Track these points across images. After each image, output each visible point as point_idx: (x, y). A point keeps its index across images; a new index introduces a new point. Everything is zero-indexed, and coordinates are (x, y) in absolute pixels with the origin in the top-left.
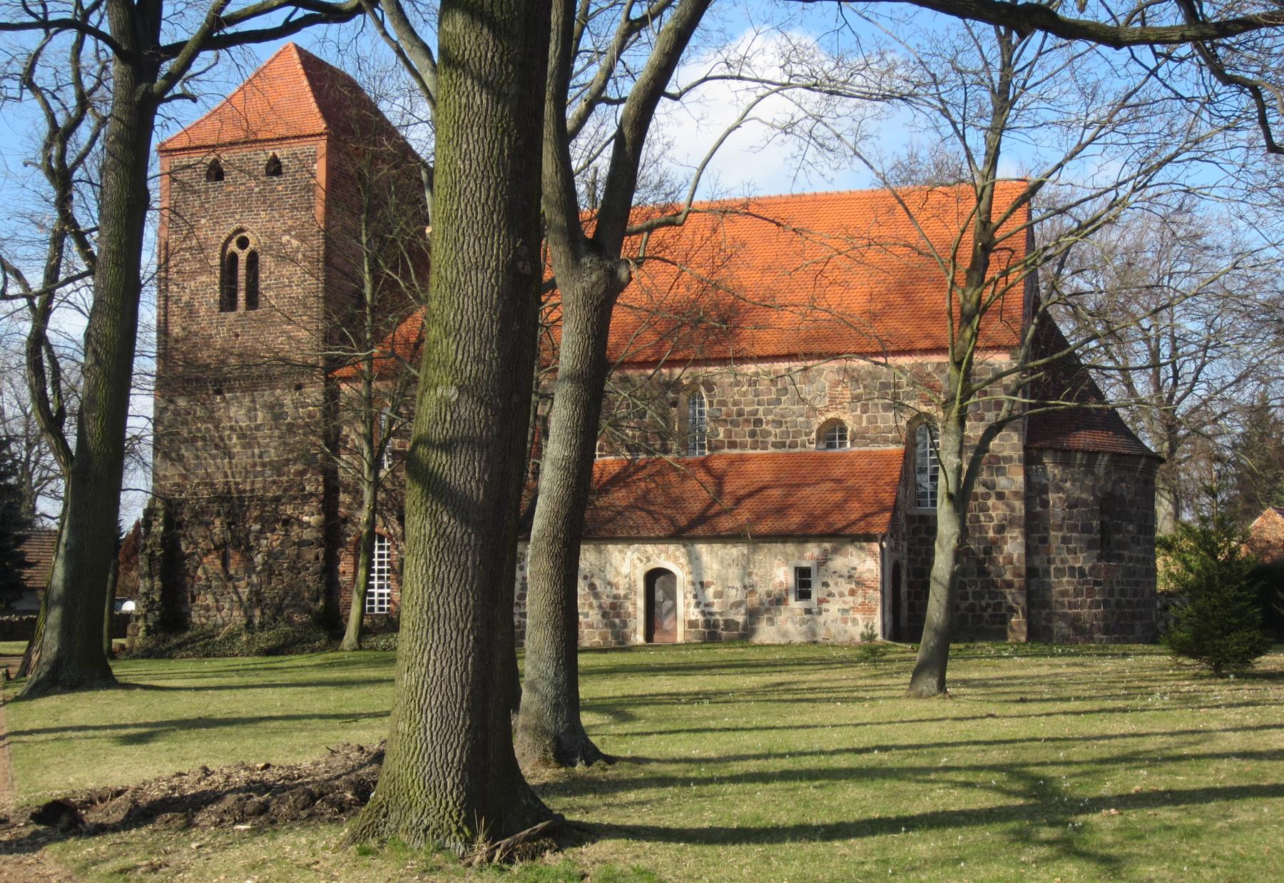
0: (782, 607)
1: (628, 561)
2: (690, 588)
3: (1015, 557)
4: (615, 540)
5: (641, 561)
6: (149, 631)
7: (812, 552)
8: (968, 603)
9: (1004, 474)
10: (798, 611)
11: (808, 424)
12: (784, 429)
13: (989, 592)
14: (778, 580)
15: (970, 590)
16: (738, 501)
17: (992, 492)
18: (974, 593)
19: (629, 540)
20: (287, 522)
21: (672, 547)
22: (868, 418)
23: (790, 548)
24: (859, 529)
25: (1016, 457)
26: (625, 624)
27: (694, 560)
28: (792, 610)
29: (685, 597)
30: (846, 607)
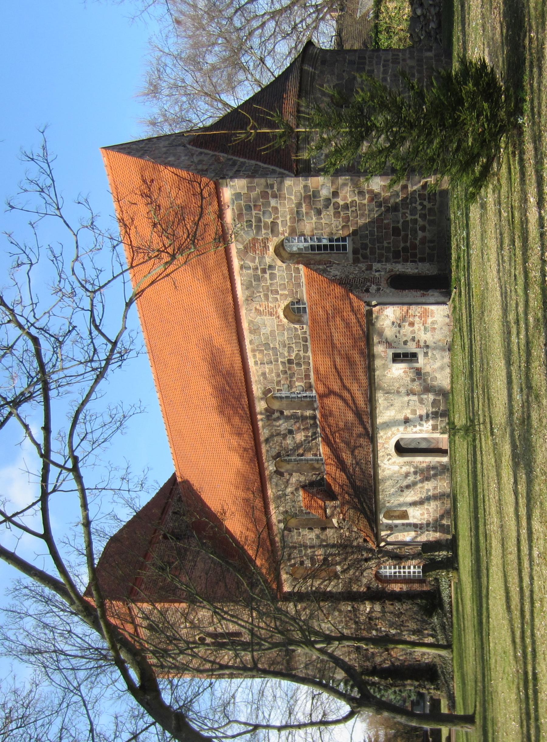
0: (423, 371)
1: (390, 467)
2: (409, 429)
3: (383, 183)
4: (376, 474)
5: (390, 459)
6: (437, 689)
7: (379, 349)
8: (419, 219)
9: (319, 192)
10: (426, 361)
11: (289, 329)
12: (294, 346)
13: (411, 203)
14: (402, 374)
15: (409, 218)
16: (344, 387)
17: (333, 201)
18: (411, 215)
19: (375, 466)
20: (370, 619)
21: (380, 441)
22: (281, 290)
23: (378, 363)
24: (364, 321)
25: (304, 183)
26: (434, 468)
27: (387, 425)
28: (425, 365)
29: (416, 433)
30: (422, 328)
